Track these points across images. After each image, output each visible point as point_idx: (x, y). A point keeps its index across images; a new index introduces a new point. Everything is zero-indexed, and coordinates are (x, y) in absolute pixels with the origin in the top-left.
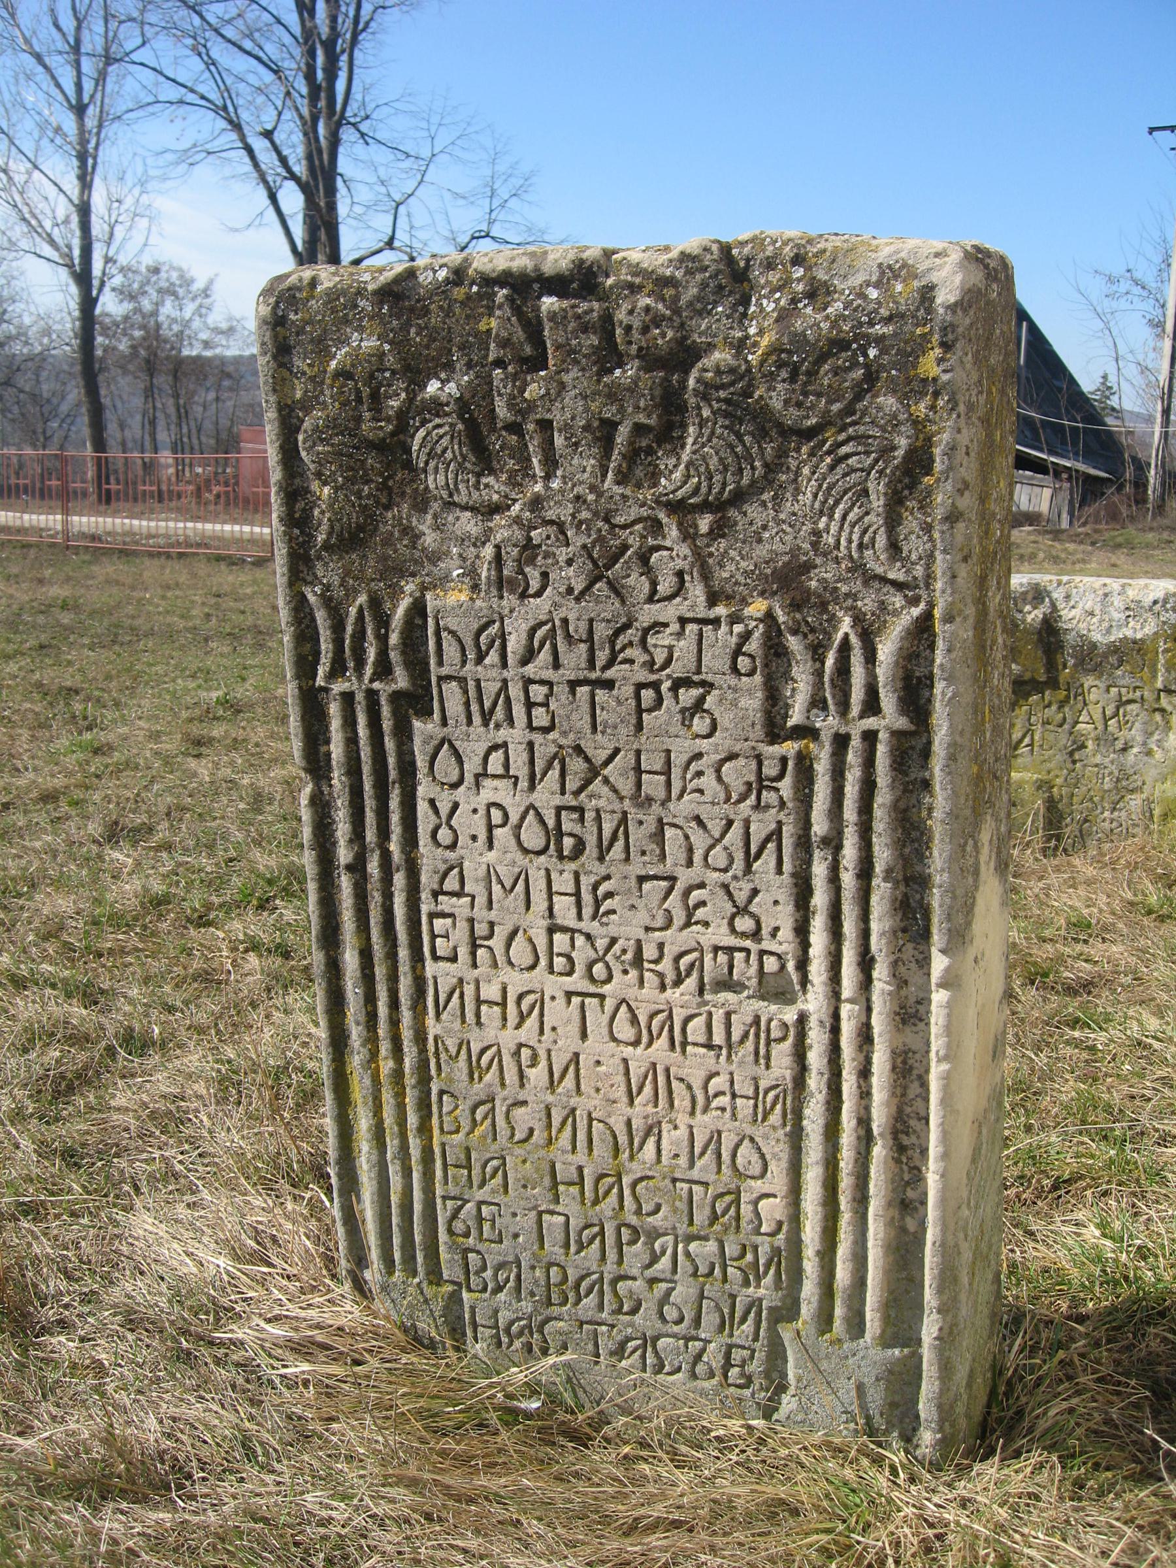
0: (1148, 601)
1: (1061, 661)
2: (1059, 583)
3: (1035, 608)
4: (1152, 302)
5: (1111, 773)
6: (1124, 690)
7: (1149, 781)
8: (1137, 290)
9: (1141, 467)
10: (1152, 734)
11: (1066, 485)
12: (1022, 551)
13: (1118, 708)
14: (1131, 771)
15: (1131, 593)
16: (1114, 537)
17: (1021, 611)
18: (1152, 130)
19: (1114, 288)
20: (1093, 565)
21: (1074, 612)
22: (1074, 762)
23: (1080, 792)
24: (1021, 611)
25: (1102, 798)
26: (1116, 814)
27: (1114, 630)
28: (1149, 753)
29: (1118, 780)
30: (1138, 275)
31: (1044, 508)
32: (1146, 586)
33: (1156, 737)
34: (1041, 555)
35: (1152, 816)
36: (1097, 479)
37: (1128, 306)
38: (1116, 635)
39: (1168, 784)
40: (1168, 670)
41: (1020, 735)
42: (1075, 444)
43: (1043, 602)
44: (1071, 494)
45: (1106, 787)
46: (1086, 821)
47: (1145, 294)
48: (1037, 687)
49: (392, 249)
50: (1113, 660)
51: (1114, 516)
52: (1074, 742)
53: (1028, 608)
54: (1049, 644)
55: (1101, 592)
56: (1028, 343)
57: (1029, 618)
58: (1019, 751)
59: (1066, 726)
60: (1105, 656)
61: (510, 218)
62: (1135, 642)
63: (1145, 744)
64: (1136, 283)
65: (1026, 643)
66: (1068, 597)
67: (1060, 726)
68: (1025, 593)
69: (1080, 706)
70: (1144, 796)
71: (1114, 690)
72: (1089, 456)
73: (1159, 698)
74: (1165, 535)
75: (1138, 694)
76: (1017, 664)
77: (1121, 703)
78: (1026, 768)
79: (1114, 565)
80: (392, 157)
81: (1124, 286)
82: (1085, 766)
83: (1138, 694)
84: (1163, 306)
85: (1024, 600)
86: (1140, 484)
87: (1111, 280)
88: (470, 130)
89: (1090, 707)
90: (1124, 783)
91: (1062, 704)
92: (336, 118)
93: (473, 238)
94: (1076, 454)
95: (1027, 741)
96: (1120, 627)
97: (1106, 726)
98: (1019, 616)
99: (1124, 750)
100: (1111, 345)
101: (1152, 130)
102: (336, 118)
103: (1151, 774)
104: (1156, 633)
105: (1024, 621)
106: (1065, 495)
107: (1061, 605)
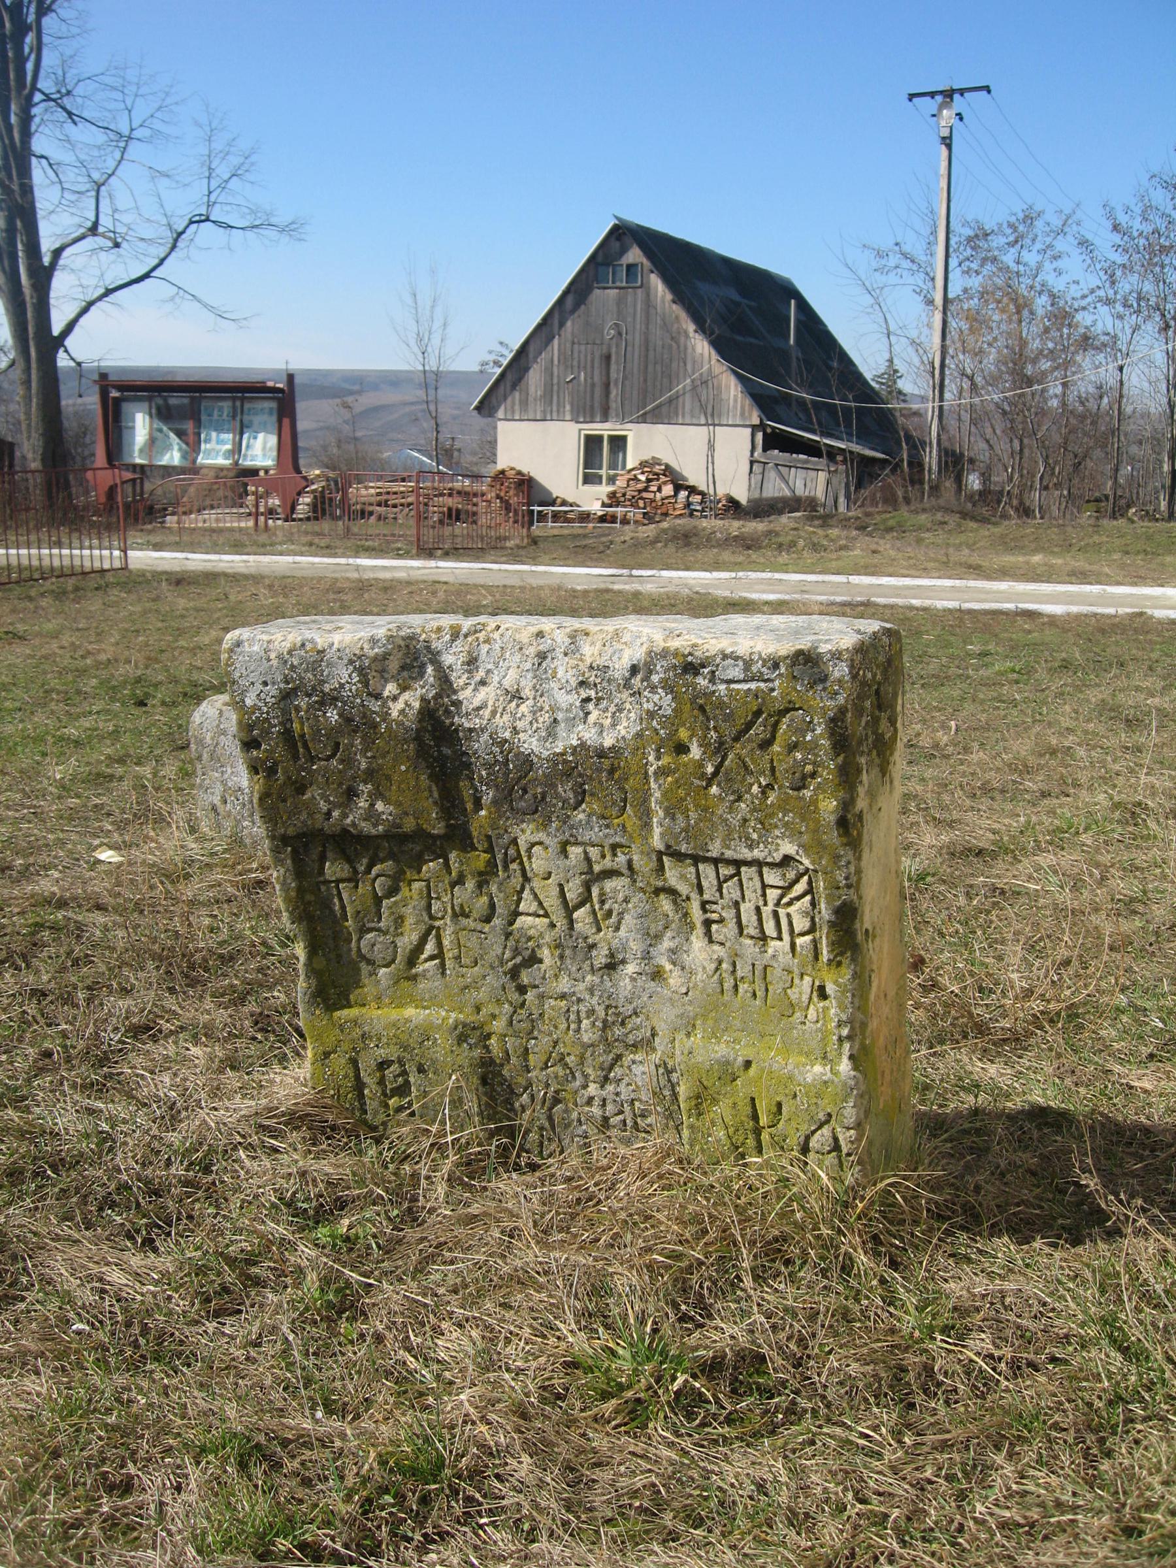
0: (620, 665)
1: (467, 793)
2: (455, 634)
3: (404, 688)
4: (922, 275)
5: (591, 1012)
6: (594, 852)
7: (662, 1029)
8: (906, 264)
9: (916, 445)
10: (658, 937)
11: (842, 468)
12: (780, 539)
13: (587, 886)
14: (628, 1009)
15: (589, 651)
16: (885, 520)
17: (378, 696)
18: (911, 97)
19: (883, 262)
20: (857, 552)
21: (483, 691)
22: (522, 990)
23: (539, 1047)
24: (378, 696)
25: (582, 1058)
26: (610, 1088)
27: (561, 730)
28: (657, 975)
29: (606, 1025)
30: (907, 248)
31: (820, 494)
32: (617, 634)
33: (667, 943)
34: (801, 543)
35: (675, 1095)
36: (873, 460)
37: (896, 280)
38: (566, 740)
39: (697, 1038)
40: (670, 813)
41: (415, 937)
42: (848, 425)
43: (422, 674)
44: (847, 476)
45: (586, 1038)
46: (556, 1101)
47: (915, 268)
48: (437, 847)
49: (95, 235)
50: (565, 790)
51: (891, 501)
52: (516, 952)
53: (390, 688)
54: (442, 760)
55: (532, 651)
56: (798, 321)
57: (395, 709)
58: (420, 969)
59: (496, 921)
60: (550, 782)
61: (230, 200)
62: (601, 753)
63: (647, 956)
64: (905, 256)
65: (396, 761)
66: (472, 662)
67: (488, 920)
68: (385, 657)
69: (516, 881)
70: (656, 1057)
71: (575, 851)
72: (863, 436)
73: (661, 869)
74: (939, 516)
75: (621, 859)
76: (387, 802)
77: (592, 877)
78: (433, 1001)
79: (874, 552)
80: (105, 138)
81: (893, 260)
82: (542, 997)
83: (621, 859)
84: (933, 279)
85: (382, 672)
86: (917, 464)
87: (880, 254)
88: (169, 101)
89: (536, 883)
90: (618, 1031)
91: (483, 879)
92: (26, 91)
93: (191, 222)
94: (850, 434)
95: (430, 948)
96: (571, 722)
97: (571, 922)
98: (375, 706)
99: (612, 966)
100: (882, 321)
101: (911, 97)
102: (26, 91)
103: (664, 1018)
104: (639, 735)
105: (386, 715)
106: (840, 481)
107: (459, 679)
